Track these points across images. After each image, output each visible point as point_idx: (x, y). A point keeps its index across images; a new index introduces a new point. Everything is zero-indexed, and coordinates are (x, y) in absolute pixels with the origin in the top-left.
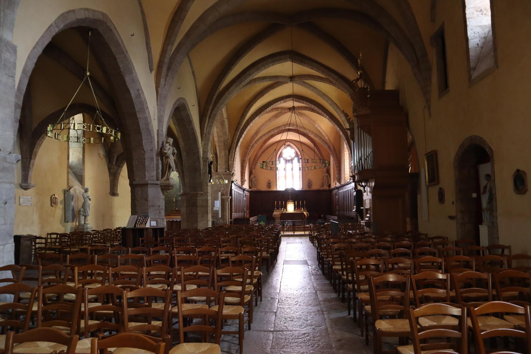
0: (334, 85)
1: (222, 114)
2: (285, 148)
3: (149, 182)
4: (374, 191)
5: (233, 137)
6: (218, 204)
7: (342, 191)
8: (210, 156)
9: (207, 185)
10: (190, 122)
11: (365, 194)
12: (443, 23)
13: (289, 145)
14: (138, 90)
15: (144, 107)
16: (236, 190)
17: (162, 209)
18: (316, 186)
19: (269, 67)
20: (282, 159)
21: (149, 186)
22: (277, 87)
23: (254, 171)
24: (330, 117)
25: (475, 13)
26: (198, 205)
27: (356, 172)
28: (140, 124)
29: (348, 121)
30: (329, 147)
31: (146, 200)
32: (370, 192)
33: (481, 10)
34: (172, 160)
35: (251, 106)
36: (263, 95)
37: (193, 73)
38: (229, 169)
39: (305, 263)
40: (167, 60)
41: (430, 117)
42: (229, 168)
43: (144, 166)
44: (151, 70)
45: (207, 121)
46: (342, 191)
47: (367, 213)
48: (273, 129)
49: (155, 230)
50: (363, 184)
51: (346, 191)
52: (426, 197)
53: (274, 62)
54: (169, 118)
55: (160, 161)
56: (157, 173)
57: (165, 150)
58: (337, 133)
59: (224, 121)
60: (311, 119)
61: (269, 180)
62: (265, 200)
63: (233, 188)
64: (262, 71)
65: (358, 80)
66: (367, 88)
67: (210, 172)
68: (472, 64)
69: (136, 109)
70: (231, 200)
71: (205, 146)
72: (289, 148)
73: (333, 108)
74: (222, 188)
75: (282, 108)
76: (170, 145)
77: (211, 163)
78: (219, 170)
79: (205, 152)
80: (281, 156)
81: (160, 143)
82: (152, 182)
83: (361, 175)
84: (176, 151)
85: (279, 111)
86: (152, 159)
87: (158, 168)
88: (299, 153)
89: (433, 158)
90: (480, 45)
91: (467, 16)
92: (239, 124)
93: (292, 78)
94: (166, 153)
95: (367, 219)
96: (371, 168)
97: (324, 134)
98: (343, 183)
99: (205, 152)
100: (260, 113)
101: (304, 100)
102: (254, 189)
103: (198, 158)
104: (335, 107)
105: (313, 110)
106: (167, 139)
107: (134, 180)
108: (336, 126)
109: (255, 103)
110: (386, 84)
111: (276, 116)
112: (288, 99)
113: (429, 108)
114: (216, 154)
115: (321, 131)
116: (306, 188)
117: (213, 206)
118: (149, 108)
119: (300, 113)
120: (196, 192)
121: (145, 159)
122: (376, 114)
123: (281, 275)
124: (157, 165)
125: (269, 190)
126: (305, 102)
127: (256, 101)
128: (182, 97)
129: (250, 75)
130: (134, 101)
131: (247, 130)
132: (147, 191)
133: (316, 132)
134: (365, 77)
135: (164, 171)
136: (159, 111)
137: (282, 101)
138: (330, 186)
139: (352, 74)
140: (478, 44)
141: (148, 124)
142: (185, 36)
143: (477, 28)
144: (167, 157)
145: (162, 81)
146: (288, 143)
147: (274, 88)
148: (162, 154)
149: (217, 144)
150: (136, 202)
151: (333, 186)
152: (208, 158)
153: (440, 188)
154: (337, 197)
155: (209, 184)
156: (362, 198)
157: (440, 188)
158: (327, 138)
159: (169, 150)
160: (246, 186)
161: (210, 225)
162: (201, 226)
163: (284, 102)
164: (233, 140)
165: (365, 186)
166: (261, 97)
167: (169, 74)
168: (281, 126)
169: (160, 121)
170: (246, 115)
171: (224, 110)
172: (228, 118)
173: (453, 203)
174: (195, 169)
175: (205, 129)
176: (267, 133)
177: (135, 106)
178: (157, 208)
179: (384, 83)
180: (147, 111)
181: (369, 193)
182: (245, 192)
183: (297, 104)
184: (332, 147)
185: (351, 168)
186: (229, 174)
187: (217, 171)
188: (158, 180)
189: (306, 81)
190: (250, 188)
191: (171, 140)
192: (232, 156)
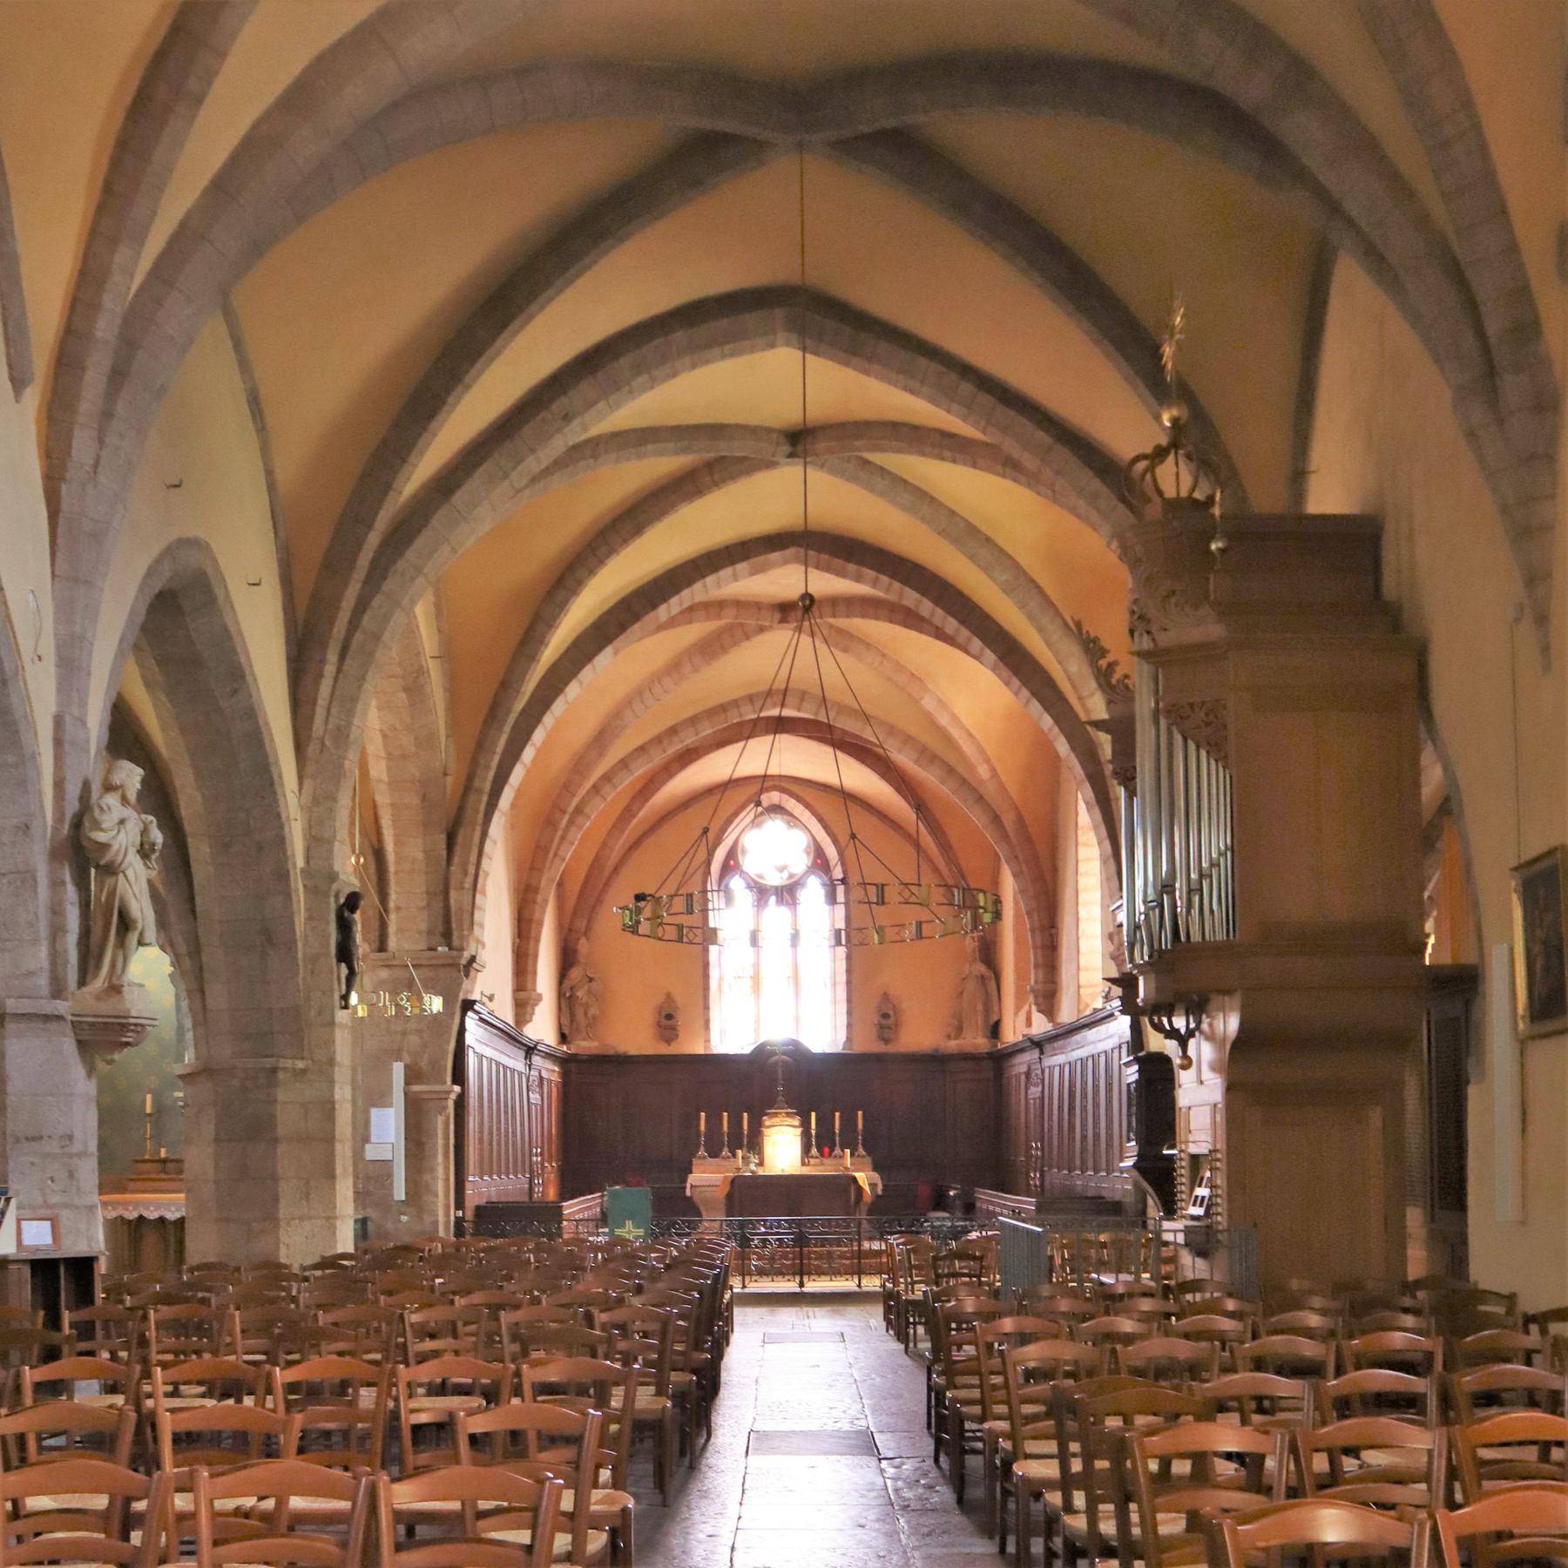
2: (756, 822)
4: (1241, 1055)
8: (348, 867)
9: (332, 1023)
10: (237, 676)
11: (1185, 1078)
13: (777, 809)
16: (488, 1052)
18: (922, 1033)
19: (674, 375)
20: (736, 883)
22: (716, 484)
23: (583, 946)
24: (1002, 658)
26: (281, 1131)
27: (1142, 955)
29: (1104, 678)
30: (996, 820)
34: (137, 884)
36: (638, 530)
37: (254, 401)
38: (447, 936)
40: (106, 327)
41: (1547, 667)
42: (449, 928)
44: (19, 383)
45: (330, 669)
46: (1060, 1059)
47: (1196, 1180)
48: (693, 721)
50: (1180, 1023)
54: (120, 655)
55: (71, 892)
56: (56, 957)
57: (97, 826)
59: (421, 671)
60: (900, 667)
61: (669, 996)
62: (637, 1109)
63: (469, 1039)
65: (1159, 454)
66: (1210, 500)
67: (345, 953)
70: (461, 1103)
71: (320, 805)
72: (775, 826)
73: (1022, 606)
74: (414, 1040)
76: (124, 800)
77: (352, 902)
78: (392, 943)
79: (318, 842)
81: (73, 790)
82: (25, 1006)
84: (157, 836)
85: (728, 618)
87: (57, 931)
88: (831, 852)
92: (507, 686)
93: (799, 440)
94: (105, 847)
97: (968, 749)
98: (1066, 1015)
99: (318, 842)
100: (623, 628)
102: (584, 1046)
103: (283, 875)
105: (911, 619)
108: (1036, 707)
109: (592, 572)
111: (710, 649)
112: (776, 556)
114: (379, 854)
115: (955, 732)
117: (363, 1136)
119: (841, 631)
120: (268, 1063)
123: (733, 1510)
124: (57, 911)
125: (665, 1050)
127: (601, 562)
131: (548, 720)
134: (1196, 438)
135: (97, 931)
137: (742, 567)
138: (995, 1030)
142: (207, 192)
145: (82, 446)
146: (774, 797)
147: (699, 492)
151: (1012, 1033)
152: (333, 877)
154: (1035, 1091)
155: (342, 1016)
158: (983, 771)
159: (123, 828)
160: (542, 1027)
163: (755, 571)
164: (470, 777)
166: (625, 542)
167: (121, 408)
168: (735, 703)
169: (71, 667)
170: (542, 641)
172: (447, 655)
174: (266, 938)
176: (658, 740)
178: (53, 1147)
181: (1207, 1074)
182: (537, 1060)
183: (824, 583)
184: (1009, 820)
187: (382, 947)
189: (877, 458)
190: (563, 1038)
191: (131, 775)
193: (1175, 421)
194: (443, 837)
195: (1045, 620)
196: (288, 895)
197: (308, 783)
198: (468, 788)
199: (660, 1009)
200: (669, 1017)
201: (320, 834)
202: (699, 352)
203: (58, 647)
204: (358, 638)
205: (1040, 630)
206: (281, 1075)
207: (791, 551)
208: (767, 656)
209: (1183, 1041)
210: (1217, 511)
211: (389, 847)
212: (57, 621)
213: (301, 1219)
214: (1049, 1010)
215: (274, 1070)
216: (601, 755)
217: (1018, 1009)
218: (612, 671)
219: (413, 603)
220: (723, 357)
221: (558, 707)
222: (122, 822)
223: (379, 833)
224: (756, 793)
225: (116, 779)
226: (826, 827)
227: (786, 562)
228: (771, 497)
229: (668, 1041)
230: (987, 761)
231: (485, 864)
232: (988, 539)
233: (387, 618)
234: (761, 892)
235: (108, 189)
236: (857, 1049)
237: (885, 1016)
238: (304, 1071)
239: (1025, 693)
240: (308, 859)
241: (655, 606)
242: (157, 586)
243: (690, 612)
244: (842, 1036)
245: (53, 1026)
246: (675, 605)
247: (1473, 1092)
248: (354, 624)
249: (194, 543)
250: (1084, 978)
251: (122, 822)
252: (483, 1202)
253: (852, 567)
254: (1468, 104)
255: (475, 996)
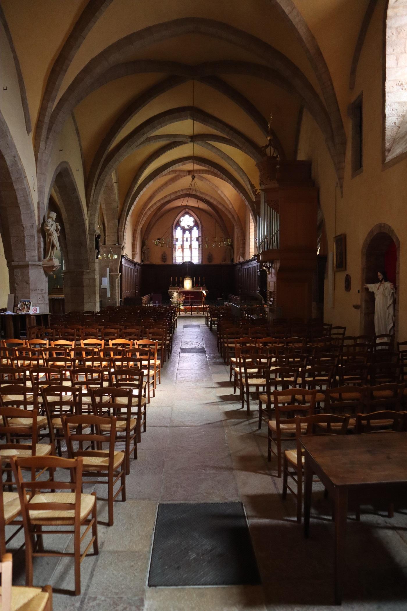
0: (241, 149)
1: (111, 178)
2: (183, 216)
3: (30, 263)
4: (279, 274)
5: (124, 204)
6: (106, 281)
7: (245, 267)
8: (97, 228)
9: (95, 262)
10: (74, 189)
11: (269, 276)
12: (362, 94)
14: (15, 157)
15: (21, 177)
16: (127, 265)
17: (45, 293)
18: (217, 260)
19: (166, 125)
20: (179, 228)
21: (30, 267)
22: (175, 147)
23: (146, 242)
24: (234, 184)
25: (395, 86)
26: (84, 284)
27: (261, 251)
28: (18, 196)
29: (254, 192)
30: (233, 216)
31: (28, 283)
32: (274, 274)
33: (402, 84)
34: (55, 237)
35: (145, 169)
36: (158, 156)
37: (77, 130)
38: (118, 242)
39: (202, 351)
40: (47, 120)
41: (342, 197)
42: (119, 239)
43: (24, 245)
44: (29, 131)
45: (94, 188)
46: (245, 267)
47: (271, 297)
48: (170, 195)
49: (38, 317)
50: (268, 265)
51: (248, 268)
52: (333, 283)
53: (172, 120)
54: (50, 188)
55: (42, 239)
56: (39, 252)
57: (47, 226)
58: (243, 201)
61: (164, 253)
62: (158, 275)
63: (123, 263)
64: (157, 129)
65: (267, 146)
66: (277, 157)
67: (97, 247)
68: (387, 145)
69: (13, 178)
71: (92, 216)
72: (187, 217)
73: (239, 173)
74: (111, 263)
75: (180, 171)
76: (52, 220)
77: (99, 236)
78: (107, 243)
79: (91, 224)
80: (178, 224)
81: (42, 218)
82: (33, 263)
83: (266, 253)
84: (59, 227)
85: (177, 173)
86: (33, 236)
87: (39, 247)
88: (199, 222)
89: (341, 241)
90: (396, 124)
91: (387, 90)
92: (131, 189)
93: (194, 138)
94: (49, 230)
95: (270, 303)
96: (276, 248)
97: (228, 202)
99: (91, 224)
100: (155, 176)
101: (205, 163)
102: (146, 262)
103: (84, 231)
104: (241, 173)
105: (216, 175)
106: (49, 214)
107: (13, 261)
108: (241, 194)
109: (149, 165)
110: (299, 152)
111: (173, 180)
113: (341, 187)
114: (104, 224)
115: (225, 198)
116: (206, 263)
117: (101, 283)
118: (28, 177)
119: (201, 176)
121: (24, 236)
122: (288, 184)
123: (177, 365)
124: (39, 243)
126: (207, 165)
127: (151, 163)
128: (66, 160)
129: (143, 134)
130: (10, 169)
131: (139, 196)
132: (28, 273)
133: (219, 200)
134: (275, 142)
135: (47, 248)
136: (39, 180)
137: (181, 164)
138: (232, 260)
139: (262, 140)
140: (395, 123)
141: (27, 196)
142: (67, 90)
143: (396, 104)
144: (50, 235)
145: (42, 145)
146: (187, 210)
147: (171, 148)
148: (43, 231)
149: (104, 212)
150: (16, 285)
151: (236, 261)
152: (95, 231)
153: (347, 275)
154: (240, 273)
155: (97, 261)
156: (267, 280)
157: (347, 275)
158: (231, 206)
159: (52, 226)
160: (137, 260)
161: (98, 310)
162: (87, 307)
163: (183, 165)
165: (270, 267)
166: (156, 159)
167: (50, 137)
168: (179, 191)
169: (41, 192)
170: (138, 180)
171: (113, 176)
172: (118, 182)
173: (359, 292)
174: (81, 244)
175: (92, 197)
176: (162, 199)
177: (11, 175)
178: (39, 292)
179: (295, 151)
180: (25, 181)
181: (273, 276)
182: (137, 266)
183: (197, 167)
184: (236, 217)
185: (256, 247)
186: (119, 248)
187: (105, 244)
188: (39, 260)
190: (142, 261)
191: (54, 215)
192: (122, 226)
193: (270, 140)
194: (117, 221)
195: (244, 177)
196: (85, 235)
197: (89, 212)
198: (122, 210)
199: (162, 255)
200: (164, 257)
201: (91, 221)
202: (172, 120)
203: (38, 188)
204: (99, 181)
205: (243, 179)
206: (84, 273)
207: (191, 161)
208: (186, 182)
209: (269, 269)
210: (278, 159)
211: (106, 225)
212: (38, 182)
213: (89, 302)
214: (244, 257)
215: (83, 272)
216: (150, 202)
217: (237, 256)
218: (152, 185)
219: (111, 173)
220: (177, 121)
221: (141, 193)
222: (52, 225)
223: (104, 220)
224: (187, 210)
225: (51, 216)
226: (198, 217)
227: (189, 163)
228: (186, 150)
229: (164, 262)
230: (231, 204)
231: (126, 226)
232: (232, 159)
233: (106, 176)
234: (184, 230)
235: (46, 89)
236: (204, 263)
237: (210, 257)
238: (89, 272)
239: (239, 192)
240: (89, 228)
241: (162, 172)
242: (58, 172)
243: (169, 173)
244: (201, 261)
245: (39, 267)
246: (166, 171)
247: (325, 281)
248: (98, 178)
249: (65, 162)
250: (251, 251)
251: (52, 225)
252: (125, 297)
253: (203, 164)
254: (330, 80)
255: (124, 254)
